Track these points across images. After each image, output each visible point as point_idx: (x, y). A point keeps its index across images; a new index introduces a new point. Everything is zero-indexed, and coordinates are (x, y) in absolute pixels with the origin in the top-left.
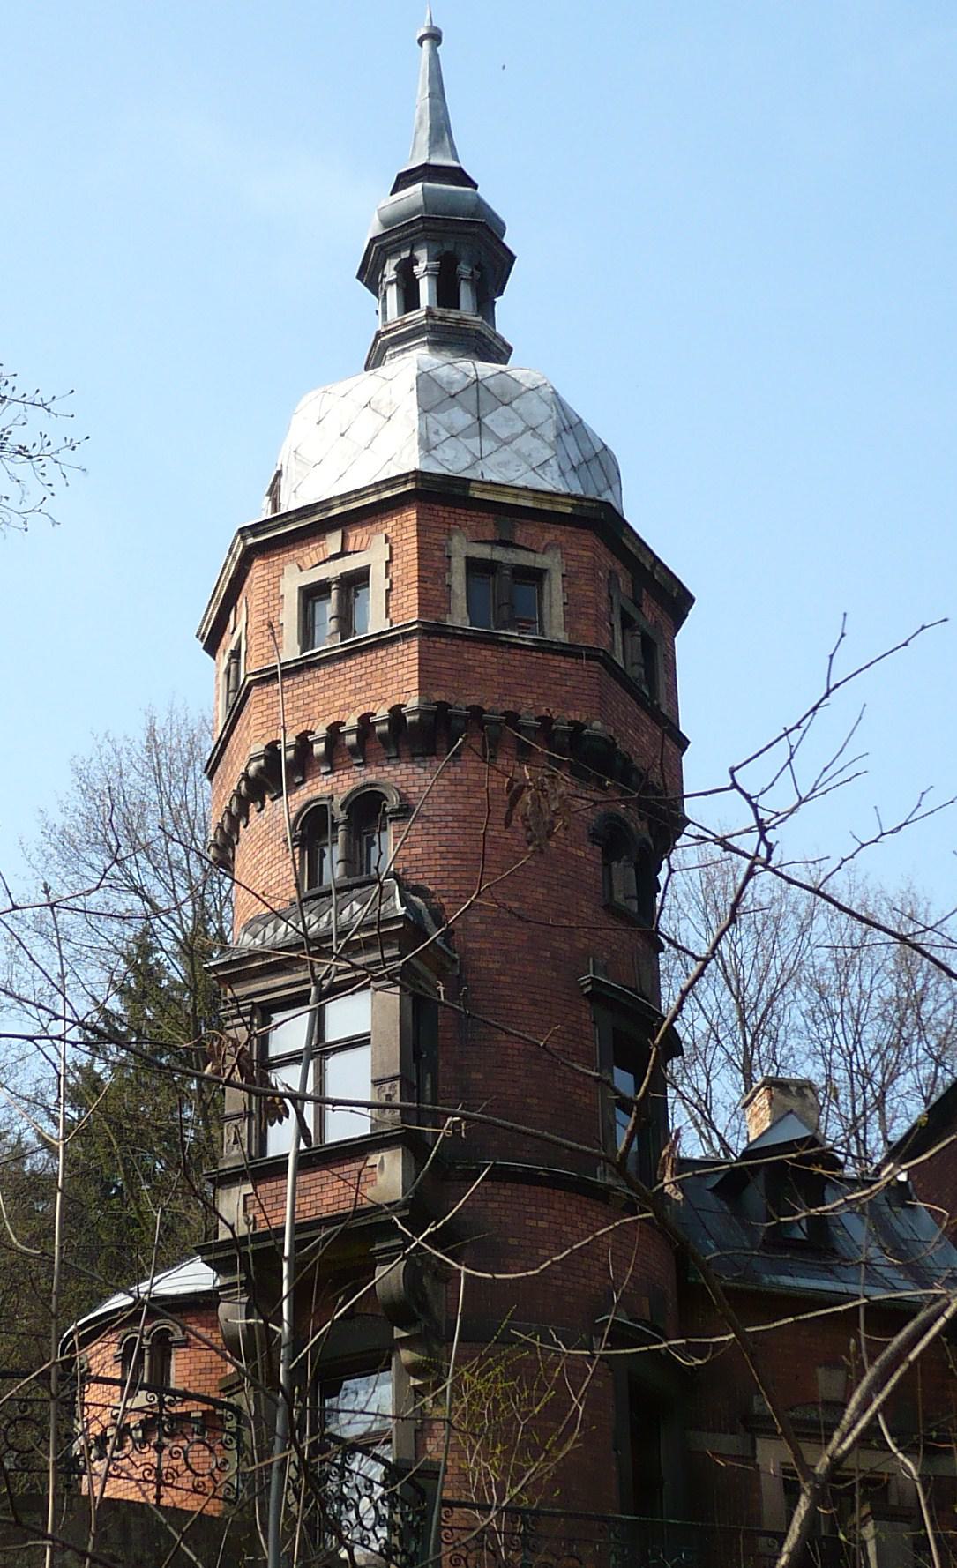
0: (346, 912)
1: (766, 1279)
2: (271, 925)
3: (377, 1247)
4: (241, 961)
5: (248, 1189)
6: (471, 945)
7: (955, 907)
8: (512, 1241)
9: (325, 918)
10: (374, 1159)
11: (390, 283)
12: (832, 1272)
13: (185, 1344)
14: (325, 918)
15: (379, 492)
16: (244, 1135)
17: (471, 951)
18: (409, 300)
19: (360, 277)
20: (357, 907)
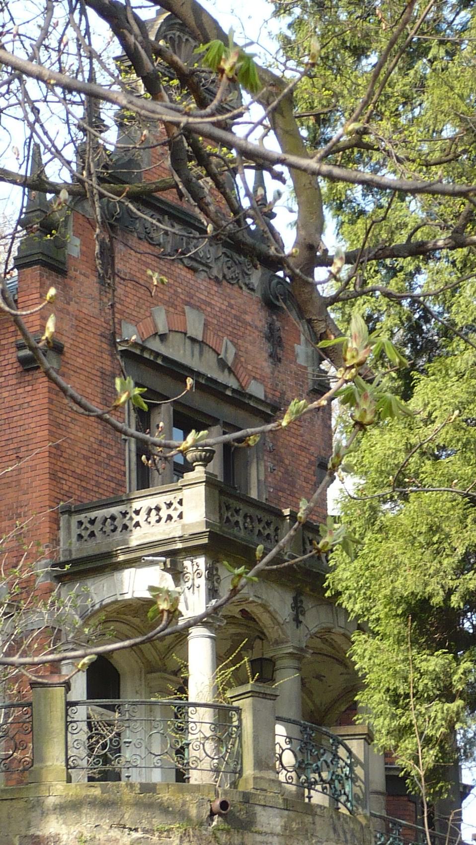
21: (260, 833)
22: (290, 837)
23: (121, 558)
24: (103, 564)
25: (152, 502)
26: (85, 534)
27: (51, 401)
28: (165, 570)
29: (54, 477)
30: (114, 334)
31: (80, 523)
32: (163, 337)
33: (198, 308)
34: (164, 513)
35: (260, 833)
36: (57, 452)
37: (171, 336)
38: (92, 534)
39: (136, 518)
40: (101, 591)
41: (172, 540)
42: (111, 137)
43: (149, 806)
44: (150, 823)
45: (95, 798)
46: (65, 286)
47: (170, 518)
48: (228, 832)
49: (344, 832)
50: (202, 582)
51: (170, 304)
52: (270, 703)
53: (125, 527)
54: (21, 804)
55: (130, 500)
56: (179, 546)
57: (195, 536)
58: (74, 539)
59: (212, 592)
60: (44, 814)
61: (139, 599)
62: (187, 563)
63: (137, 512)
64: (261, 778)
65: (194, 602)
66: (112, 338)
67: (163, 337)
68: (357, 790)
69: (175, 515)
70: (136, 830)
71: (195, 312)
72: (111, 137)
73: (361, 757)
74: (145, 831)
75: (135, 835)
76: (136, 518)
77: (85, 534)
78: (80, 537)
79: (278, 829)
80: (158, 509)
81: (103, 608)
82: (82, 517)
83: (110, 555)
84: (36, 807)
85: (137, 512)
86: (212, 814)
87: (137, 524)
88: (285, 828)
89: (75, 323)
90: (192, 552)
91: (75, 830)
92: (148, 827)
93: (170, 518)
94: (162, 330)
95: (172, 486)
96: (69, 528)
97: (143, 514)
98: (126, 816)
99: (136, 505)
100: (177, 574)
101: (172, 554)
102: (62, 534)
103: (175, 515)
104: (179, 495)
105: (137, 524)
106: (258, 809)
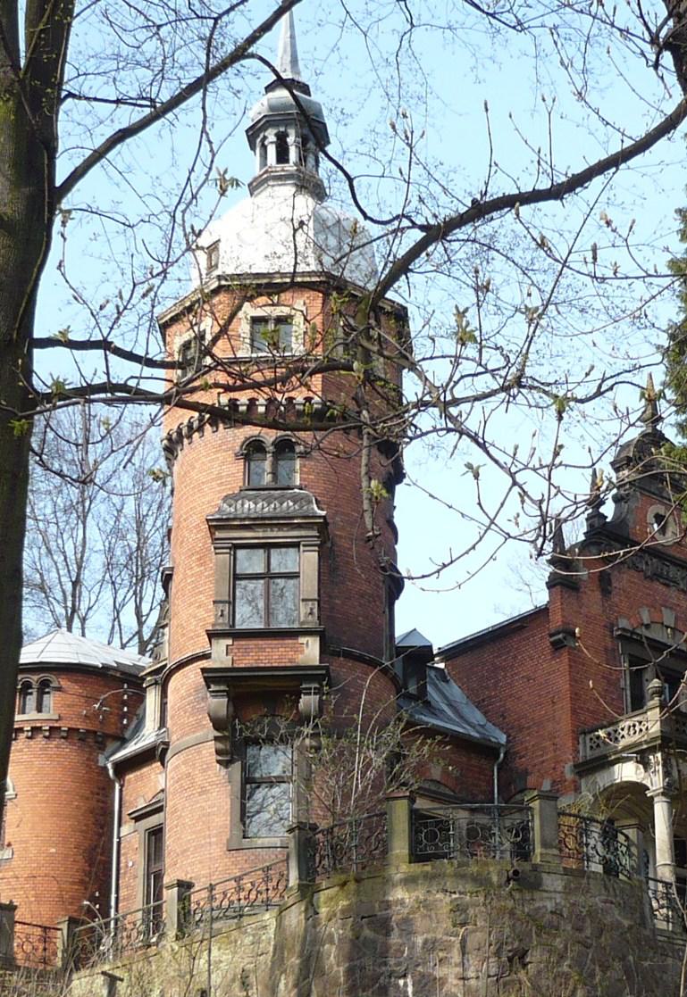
0: (285, 504)
1: (417, 717)
2: (240, 502)
3: (304, 686)
4: (227, 519)
5: (230, 642)
6: (338, 533)
7: (68, 350)
8: (352, 690)
9: (273, 506)
10: (302, 640)
11: (272, 143)
12: (433, 713)
13: (59, 689)
14: (273, 506)
15: (304, 276)
16: (226, 613)
17: (336, 535)
18: (282, 157)
19: (247, 131)
20: (291, 504)
21: (546, 891)
22: (569, 893)
23: (613, 757)
24: (604, 762)
25: (629, 723)
26: (594, 746)
27: (570, 667)
28: (637, 762)
29: (574, 711)
30: (612, 625)
31: (591, 739)
32: (647, 626)
33: (671, 608)
34: (637, 729)
35: (546, 891)
36: (575, 696)
37: (653, 625)
38: (598, 746)
39: (622, 733)
40: (602, 780)
41: (641, 744)
42: (608, 510)
43: (463, 876)
44: (464, 887)
45: (427, 872)
46: (578, 597)
47: (641, 730)
48: (521, 891)
49: (614, 890)
50: (660, 768)
51: (652, 606)
52: (553, 803)
53: (616, 739)
54: (380, 880)
55: (617, 722)
56: (645, 747)
57: (654, 739)
58: (588, 749)
59: (667, 774)
60: (394, 886)
61: (626, 782)
62: (651, 757)
63: (623, 729)
64: (547, 854)
65: (655, 781)
66: (611, 627)
67: (647, 626)
68: (633, 863)
69: (644, 729)
70: (455, 893)
71: (668, 610)
72: (608, 510)
73: (635, 840)
74: (460, 893)
75: (454, 896)
76: (622, 733)
77: (594, 746)
78: (591, 747)
79: (560, 889)
80: (634, 726)
81: (605, 789)
82: (592, 735)
83: (606, 757)
84: (387, 882)
85: (623, 729)
86: (509, 880)
87: (623, 737)
88: (565, 888)
89: (586, 619)
90: (653, 750)
91: (414, 895)
92: (462, 890)
93: (641, 730)
94: (646, 622)
95: (641, 711)
96: (585, 742)
97: (626, 730)
98: (448, 884)
99: (622, 725)
100: (646, 765)
101: (641, 752)
102: (581, 747)
103: (644, 729)
104: (645, 716)
105: (623, 737)
106: (545, 876)
